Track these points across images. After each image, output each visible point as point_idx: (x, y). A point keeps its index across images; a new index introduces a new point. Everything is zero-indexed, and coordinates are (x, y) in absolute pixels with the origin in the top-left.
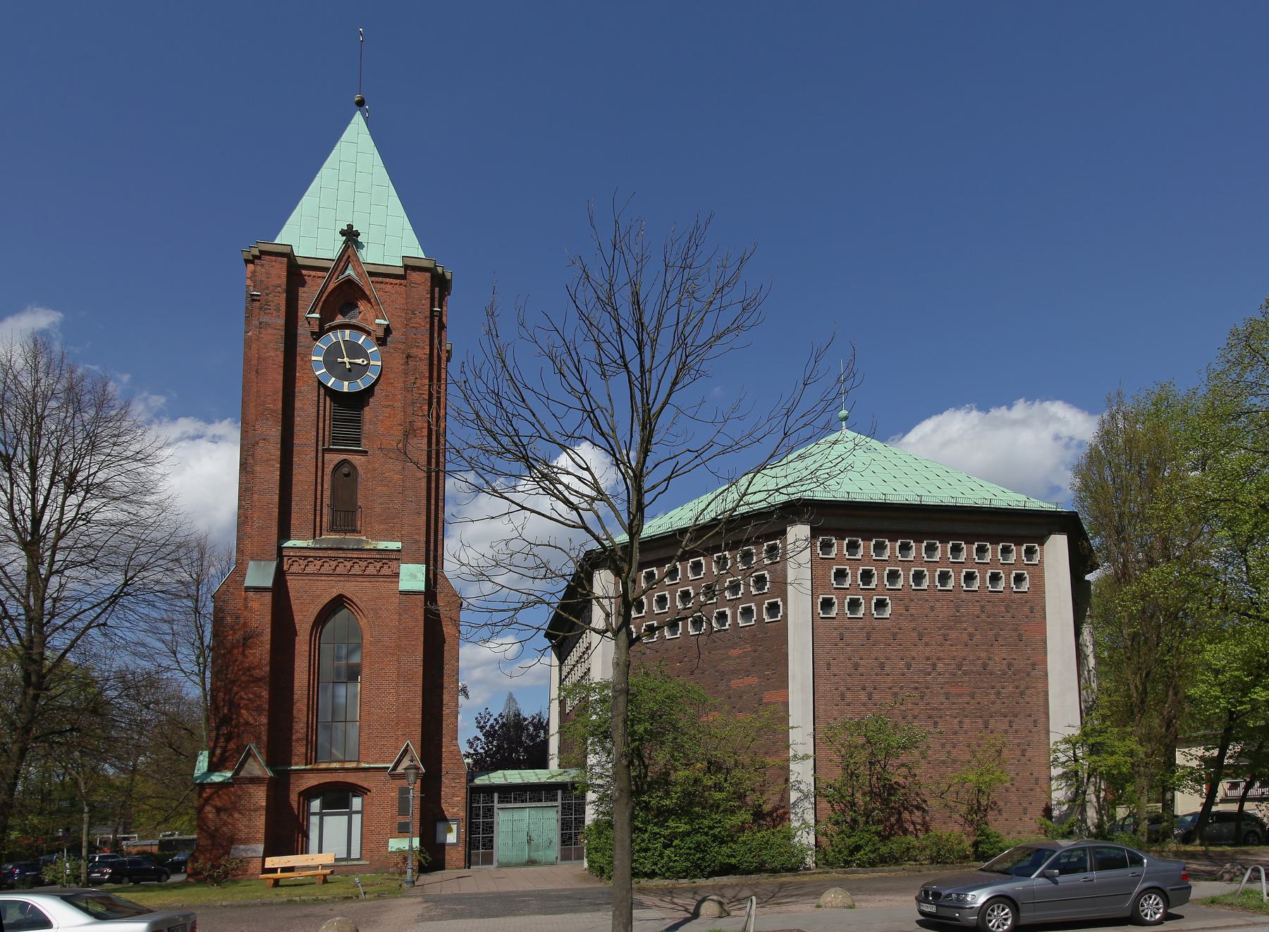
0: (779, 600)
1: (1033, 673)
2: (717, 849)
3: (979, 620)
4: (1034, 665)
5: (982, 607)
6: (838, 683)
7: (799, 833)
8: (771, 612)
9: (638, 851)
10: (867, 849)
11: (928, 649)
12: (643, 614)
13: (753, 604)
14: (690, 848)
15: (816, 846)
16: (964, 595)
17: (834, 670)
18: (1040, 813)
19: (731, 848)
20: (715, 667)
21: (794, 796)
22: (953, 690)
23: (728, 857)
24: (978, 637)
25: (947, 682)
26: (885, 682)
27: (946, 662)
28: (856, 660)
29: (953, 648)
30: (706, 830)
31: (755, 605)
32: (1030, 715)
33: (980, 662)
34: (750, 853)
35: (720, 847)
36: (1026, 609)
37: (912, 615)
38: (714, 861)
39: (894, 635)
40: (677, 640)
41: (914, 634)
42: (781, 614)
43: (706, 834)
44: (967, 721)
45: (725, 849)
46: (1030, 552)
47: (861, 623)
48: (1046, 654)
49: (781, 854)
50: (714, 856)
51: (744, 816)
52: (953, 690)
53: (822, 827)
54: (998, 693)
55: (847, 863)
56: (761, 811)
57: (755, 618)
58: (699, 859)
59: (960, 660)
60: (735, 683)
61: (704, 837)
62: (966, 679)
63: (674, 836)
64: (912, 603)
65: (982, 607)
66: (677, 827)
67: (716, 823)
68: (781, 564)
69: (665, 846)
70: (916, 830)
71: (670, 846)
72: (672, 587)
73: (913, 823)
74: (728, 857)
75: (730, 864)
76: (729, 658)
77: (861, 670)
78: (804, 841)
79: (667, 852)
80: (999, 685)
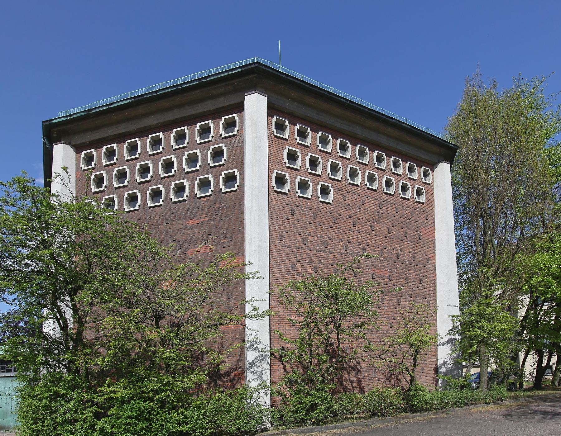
0: (236, 170)
1: (428, 265)
2: (164, 416)
3: (394, 218)
4: (428, 259)
5: (397, 208)
6: (289, 254)
7: (256, 395)
8: (227, 184)
9: (62, 424)
10: (323, 407)
11: (360, 236)
12: (103, 188)
13: (210, 176)
14: (130, 417)
15: (272, 406)
16: (385, 197)
17: (286, 242)
18: (432, 371)
19: (182, 413)
20: (173, 236)
21: (250, 356)
22: (377, 272)
23: (179, 424)
24: (393, 232)
25: (373, 265)
26: (328, 259)
27: (373, 248)
28: (305, 235)
29: (377, 238)
30: (151, 394)
31: (212, 177)
32: (425, 298)
33: (395, 252)
34: (204, 418)
35: (169, 414)
36: (423, 216)
37: (348, 205)
38: (162, 430)
39: (335, 219)
40: (136, 212)
41: (350, 221)
42: (238, 184)
43: (151, 400)
44: (386, 298)
45: (175, 416)
46: (426, 174)
47: (309, 203)
48: (435, 253)
49: (238, 418)
50: (162, 425)
51: (198, 377)
52: (377, 272)
53: (275, 388)
54: (406, 278)
55: (303, 422)
56: (218, 371)
57: (212, 189)
58: (142, 429)
59: (382, 248)
60: (192, 252)
61: (148, 405)
62: (386, 264)
63: (110, 402)
64: (349, 195)
65: (397, 208)
66: (114, 392)
67: (164, 386)
68: (238, 138)
69: (98, 416)
70: (353, 387)
71: (105, 415)
72: (132, 162)
73: (352, 382)
74: (179, 424)
75: (182, 432)
76: (186, 228)
77: (309, 245)
78: (261, 401)
79: (100, 423)
80: (406, 272)
